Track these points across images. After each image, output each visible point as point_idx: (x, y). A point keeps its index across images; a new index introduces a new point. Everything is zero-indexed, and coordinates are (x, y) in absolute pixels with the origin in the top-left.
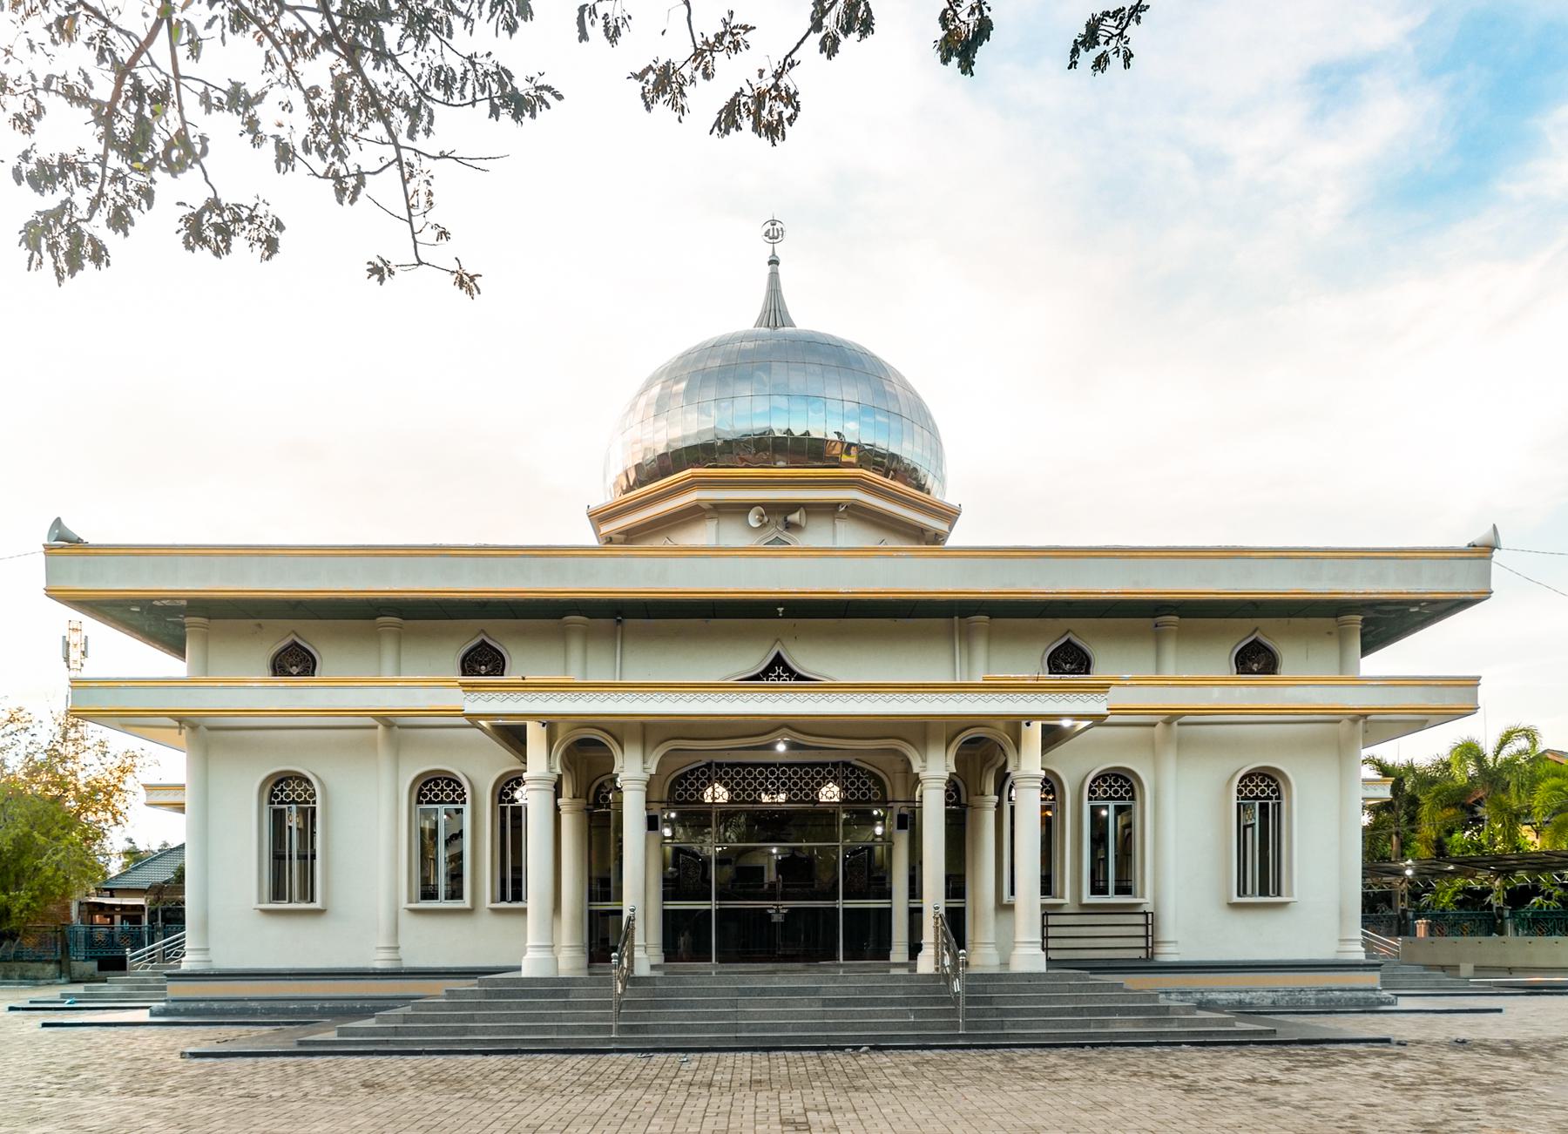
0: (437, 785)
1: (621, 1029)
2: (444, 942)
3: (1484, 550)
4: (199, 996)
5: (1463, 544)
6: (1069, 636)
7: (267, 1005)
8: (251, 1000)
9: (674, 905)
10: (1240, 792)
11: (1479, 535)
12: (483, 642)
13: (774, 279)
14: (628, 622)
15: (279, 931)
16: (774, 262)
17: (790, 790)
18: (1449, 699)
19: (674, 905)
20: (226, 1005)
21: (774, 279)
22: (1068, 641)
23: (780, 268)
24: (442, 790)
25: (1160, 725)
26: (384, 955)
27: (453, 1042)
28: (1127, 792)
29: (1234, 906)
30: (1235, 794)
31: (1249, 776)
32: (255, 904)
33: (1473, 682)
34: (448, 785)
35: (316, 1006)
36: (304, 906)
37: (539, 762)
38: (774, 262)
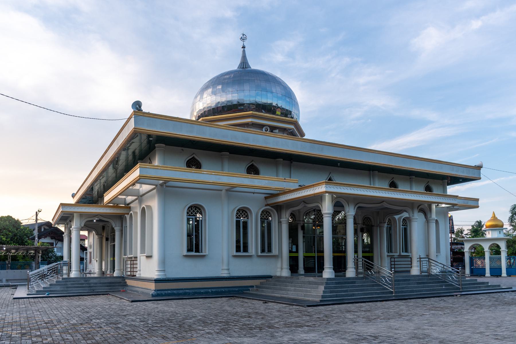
0: (192, 209)
1: (396, 292)
2: (251, 267)
3: (479, 167)
4: (166, 288)
5: (474, 165)
6: (194, 155)
7: (193, 291)
8: (185, 289)
9: (336, 254)
10: (188, 213)
11: (477, 163)
12: (193, 157)
13: (244, 51)
14: (294, 163)
15: (190, 263)
16: (244, 47)
17: (196, 213)
18: (471, 203)
19: (336, 254)
20: (217, 290)
21: (244, 51)
22: (193, 157)
23: (245, 49)
24: (194, 211)
25: (224, 191)
26: (226, 272)
27: (417, 295)
28: (246, 216)
29: (235, 256)
30: (235, 217)
31: (191, 207)
32: (185, 253)
33: (477, 200)
34: (243, 212)
35: (175, 292)
36: (197, 254)
37: (350, 212)
38: (244, 47)
